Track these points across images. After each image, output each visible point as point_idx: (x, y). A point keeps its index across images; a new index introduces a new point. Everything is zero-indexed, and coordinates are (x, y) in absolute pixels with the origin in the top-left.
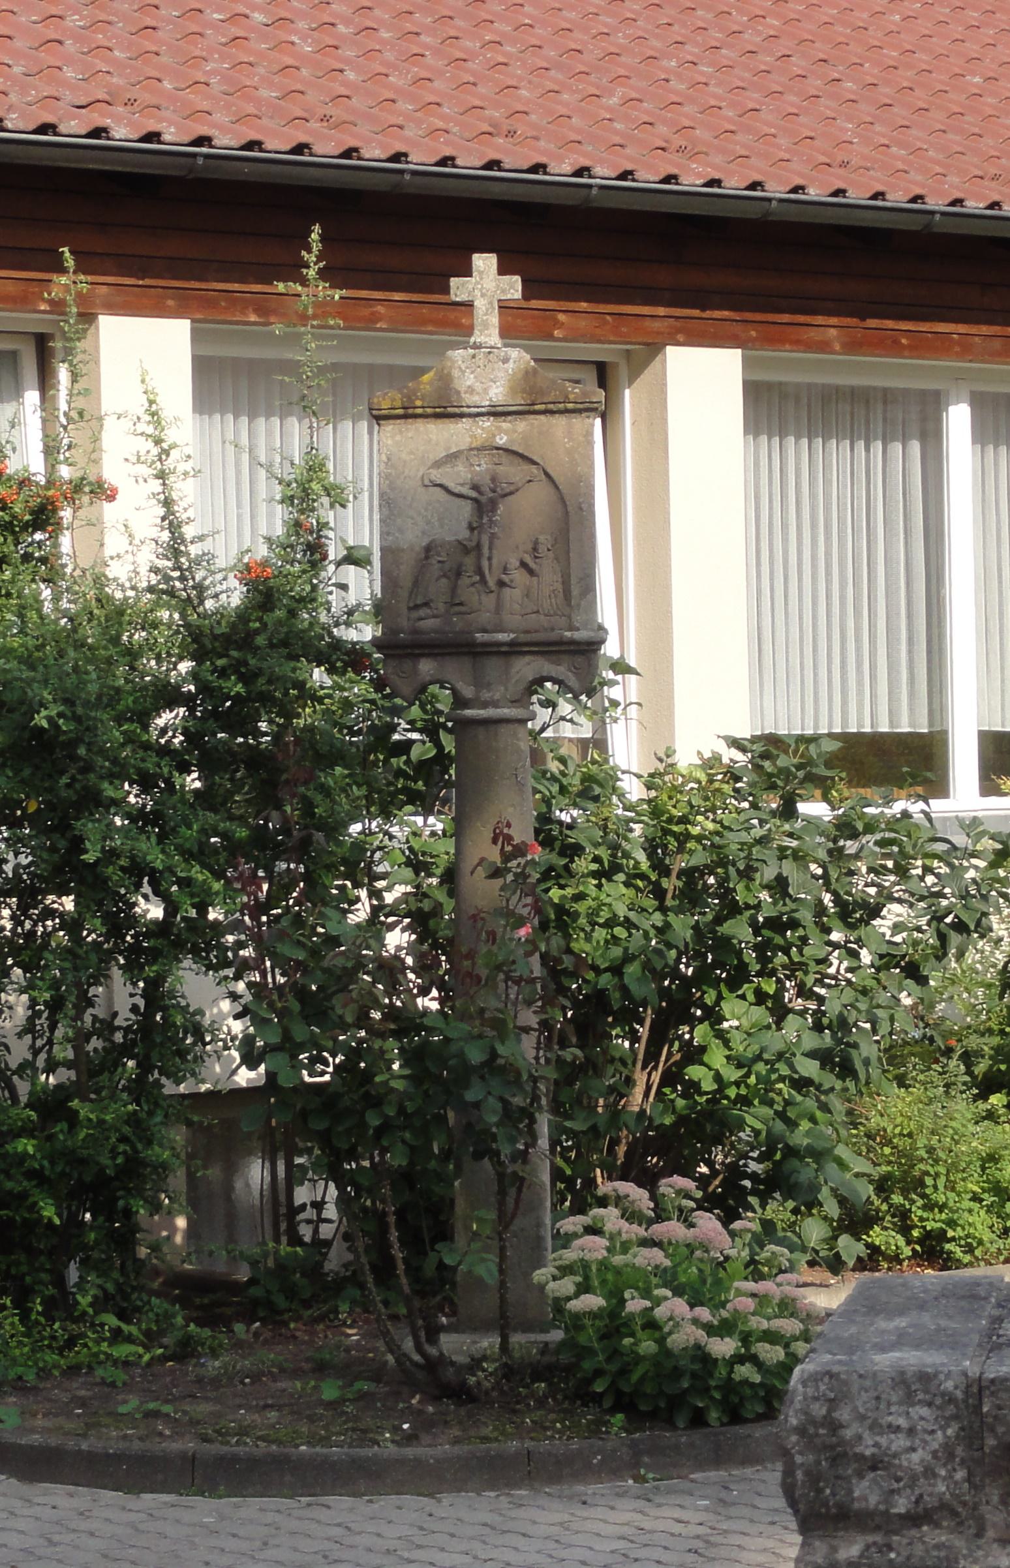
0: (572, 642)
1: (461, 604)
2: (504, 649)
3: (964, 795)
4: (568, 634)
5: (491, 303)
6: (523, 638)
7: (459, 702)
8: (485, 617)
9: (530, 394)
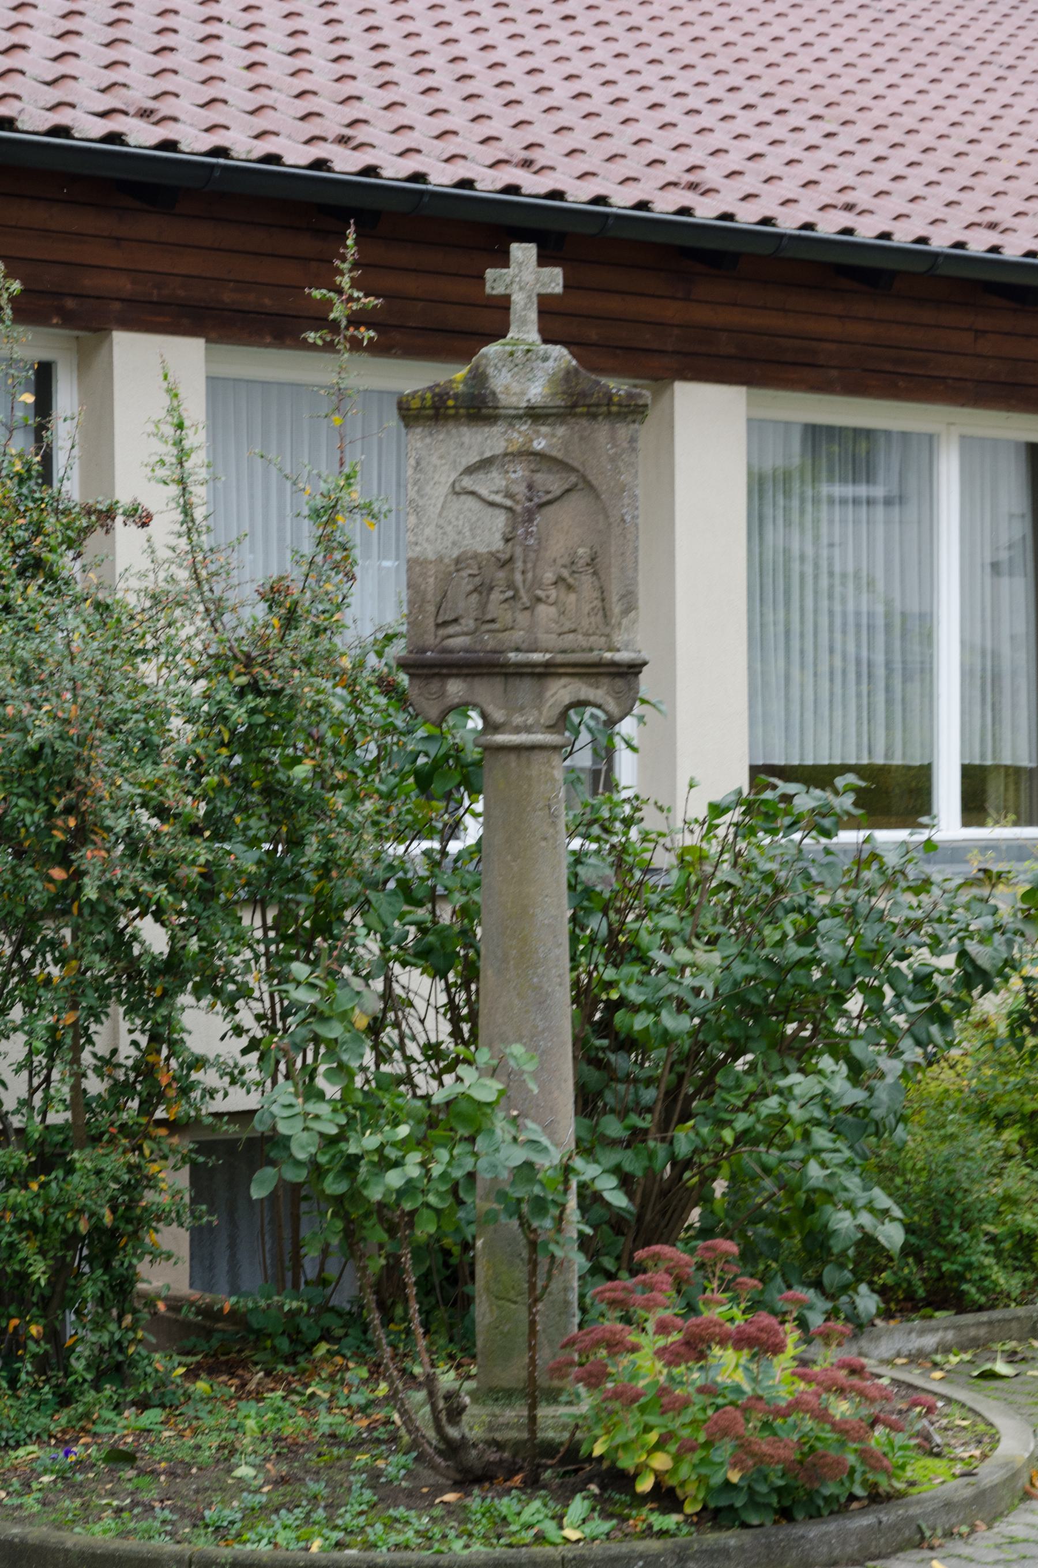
0: (613, 664)
1: (493, 621)
2: (538, 670)
3: (947, 820)
4: (608, 655)
5: (529, 297)
6: (560, 658)
7: (491, 726)
8: (517, 636)
9: (571, 395)
